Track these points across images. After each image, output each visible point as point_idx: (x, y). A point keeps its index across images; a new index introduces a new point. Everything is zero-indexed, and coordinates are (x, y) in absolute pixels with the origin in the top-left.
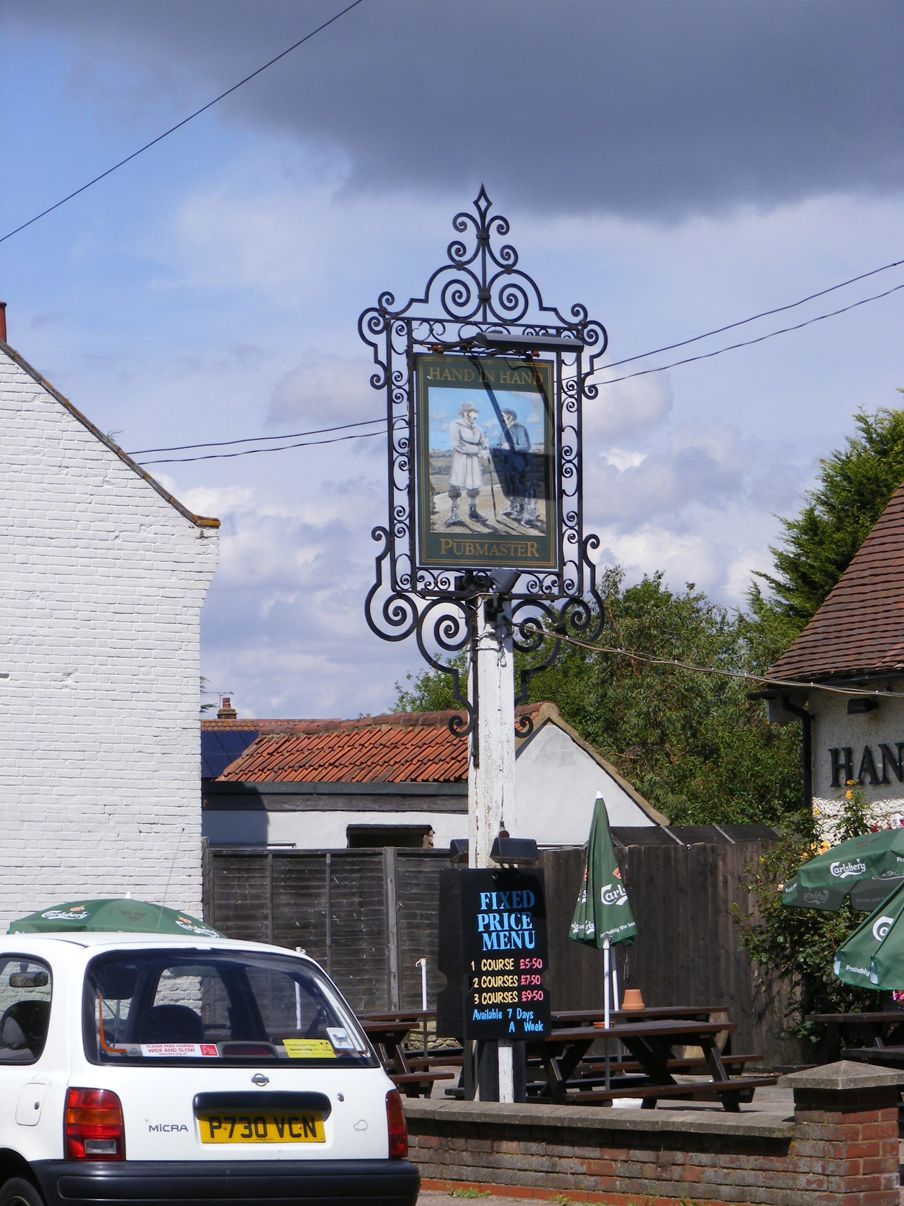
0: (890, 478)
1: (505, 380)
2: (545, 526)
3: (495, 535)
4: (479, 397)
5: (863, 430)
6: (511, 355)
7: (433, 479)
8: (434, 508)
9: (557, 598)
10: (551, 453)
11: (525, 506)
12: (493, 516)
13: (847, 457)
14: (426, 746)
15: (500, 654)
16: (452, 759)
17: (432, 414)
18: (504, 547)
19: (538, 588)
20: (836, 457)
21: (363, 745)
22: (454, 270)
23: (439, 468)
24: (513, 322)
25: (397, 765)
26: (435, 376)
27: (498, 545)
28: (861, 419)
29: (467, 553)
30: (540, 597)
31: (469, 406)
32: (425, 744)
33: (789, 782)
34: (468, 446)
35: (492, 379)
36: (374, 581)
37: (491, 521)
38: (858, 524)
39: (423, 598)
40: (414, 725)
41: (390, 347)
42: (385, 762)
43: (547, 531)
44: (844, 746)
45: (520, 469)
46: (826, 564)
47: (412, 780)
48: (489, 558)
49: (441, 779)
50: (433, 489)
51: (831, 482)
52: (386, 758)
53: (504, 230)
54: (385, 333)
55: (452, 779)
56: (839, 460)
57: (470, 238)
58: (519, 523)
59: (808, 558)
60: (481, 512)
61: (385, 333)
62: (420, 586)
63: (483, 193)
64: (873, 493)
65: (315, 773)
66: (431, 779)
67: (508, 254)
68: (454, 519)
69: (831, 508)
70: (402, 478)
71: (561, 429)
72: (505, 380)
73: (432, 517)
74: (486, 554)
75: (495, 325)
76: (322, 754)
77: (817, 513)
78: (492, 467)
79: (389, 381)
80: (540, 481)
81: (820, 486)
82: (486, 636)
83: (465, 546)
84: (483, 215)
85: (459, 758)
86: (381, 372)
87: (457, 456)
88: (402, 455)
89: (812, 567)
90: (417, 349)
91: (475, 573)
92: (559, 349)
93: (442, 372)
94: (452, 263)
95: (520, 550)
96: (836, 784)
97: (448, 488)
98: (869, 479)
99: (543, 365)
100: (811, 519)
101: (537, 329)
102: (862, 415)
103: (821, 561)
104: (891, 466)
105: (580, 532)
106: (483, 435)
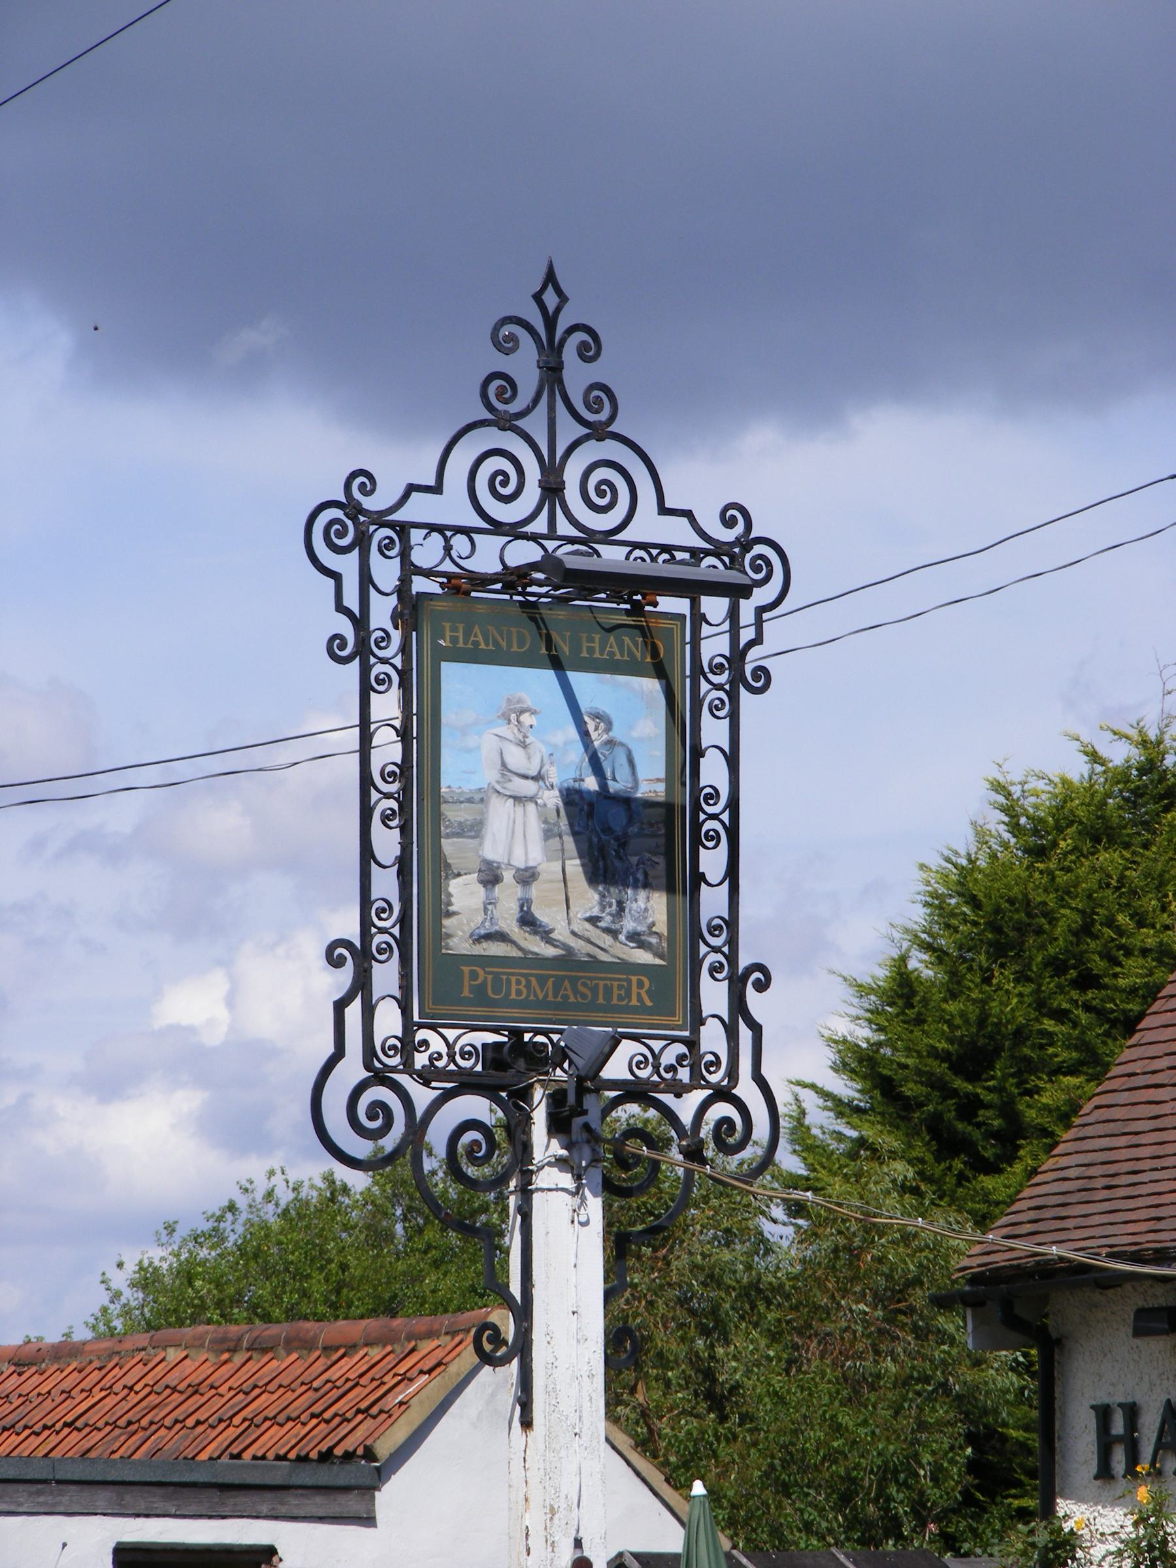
0: (1051, 900)
1: (591, 650)
2: (665, 945)
3: (567, 960)
4: (537, 684)
5: (1005, 810)
6: (601, 602)
7: (448, 845)
8: (450, 904)
9: (689, 1088)
10: (677, 801)
11: (627, 905)
12: (564, 923)
13: (970, 861)
14: (257, 1391)
15: (577, 1200)
16: (313, 1416)
17: (448, 715)
18: (585, 985)
19: (650, 1069)
20: (948, 860)
21: (131, 1388)
22: (494, 430)
23: (460, 823)
24: (608, 537)
25: (201, 1429)
26: (454, 640)
27: (573, 981)
28: (999, 787)
29: (513, 996)
30: (655, 1087)
31: (520, 701)
32: (255, 1387)
33: (896, 1472)
34: (517, 781)
35: (565, 649)
36: (330, 1049)
37: (561, 933)
38: (990, 985)
39: (426, 1083)
40: (234, 1350)
41: (366, 580)
42: (176, 1421)
43: (669, 956)
44: (1122, 1400)
45: (618, 830)
46: (929, 1061)
47: (233, 1457)
48: (557, 1006)
49: (292, 1455)
50: (448, 866)
51: (940, 907)
52: (179, 1414)
53: (590, 352)
54: (356, 552)
55: (314, 1455)
56: (955, 866)
57: (524, 366)
58: (615, 938)
59: (895, 1049)
60: (541, 914)
61: (356, 552)
62: (421, 1060)
63: (550, 278)
64: (1020, 928)
65: (34, 1441)
66: (271, 1455)
67: (598, 400)
68: (488, 928)
69: (939, 955)
70: (386, 842)
71: (698, 753)
72: (591, 650)
73: (446, 922)
74: (550, 998)
75: (571, 540)
76: (48, 1404)
77: (912, 964)
78: (564, 823)
79: (363, 650)
80: (656, 854)
81: (918, 916)
82: (549, 1164)
83: (509, 982)
84: (550, 322)
85: (327, 1415)
86: (346, 628)
87: (495, 801)
88: (388, 796)
89: (905, 1067)
90: (420, 584)
91: (527, 1037)
92: (693, 589)
93: (468, 633)
94: (489, 416)
95: (616, 992)
96: (1104, 1473)
97: (476, 865)
98: (1011, 901)
99: (664, 624)
100: (901, 974)
101: (654, 552)
102: (1002, 780)
103: (920, 1056)
104: (1053, 879)
105: (732, 958)
106: (546, 760)
